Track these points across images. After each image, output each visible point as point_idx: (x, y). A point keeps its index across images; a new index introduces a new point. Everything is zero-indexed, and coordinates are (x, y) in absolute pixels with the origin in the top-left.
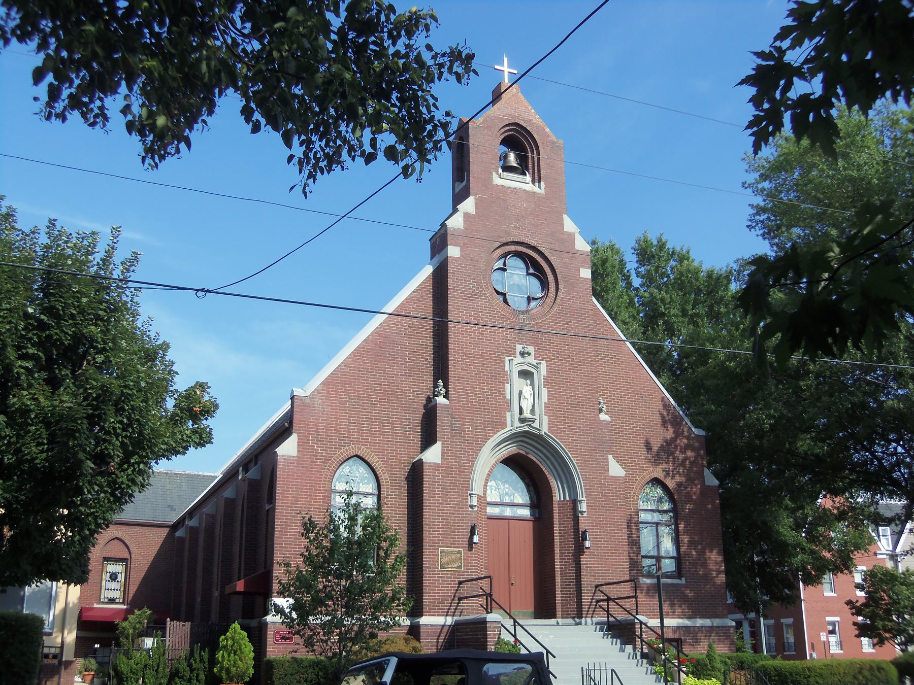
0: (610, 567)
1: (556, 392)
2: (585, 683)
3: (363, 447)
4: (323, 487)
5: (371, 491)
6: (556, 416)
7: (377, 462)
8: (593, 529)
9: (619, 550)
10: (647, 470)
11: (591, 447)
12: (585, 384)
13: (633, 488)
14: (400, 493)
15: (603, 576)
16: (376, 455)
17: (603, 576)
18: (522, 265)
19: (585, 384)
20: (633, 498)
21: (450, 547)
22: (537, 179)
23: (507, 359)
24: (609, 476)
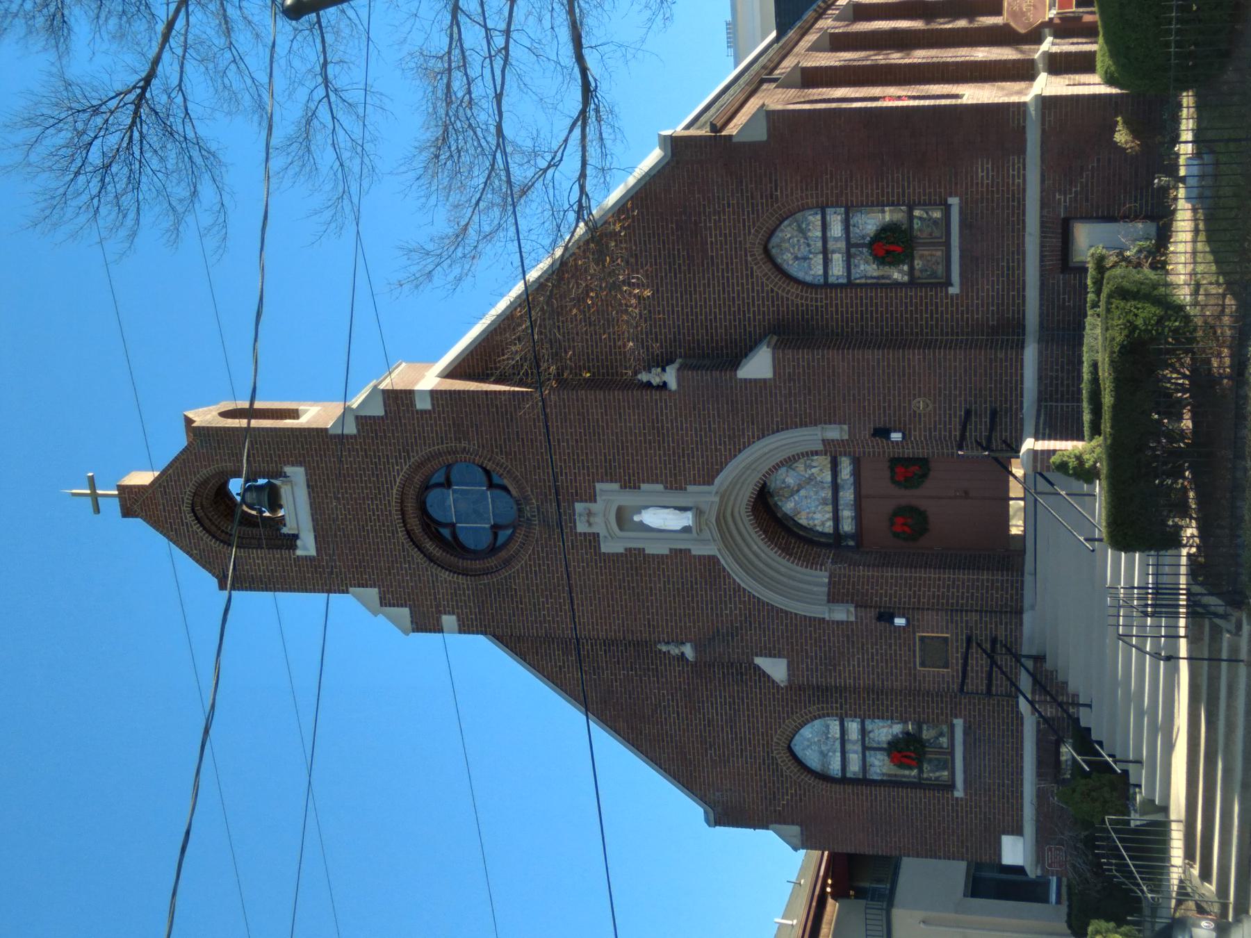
0: (935, 387)
1: (643, 468)
2: (826, 930)
3: (775, 740)
4: (821, 302)
5: (819, 217)
6: (685, 471)
7: (795, 721)
8: (869, 414)
9: (904, 367)
10: (752, 268)
11: (728, 411)
12: (620, 414)
13: (788, 299)
14: (829, 381)
15: (950, 400)
16: (784, 722)
17: (950, 400)
18: (462, 537)
19: (620, 414)
20: (806, 300)
21: (914, 651)
22: (189, 421)
23: (579, 507)
24: (775, 379)
